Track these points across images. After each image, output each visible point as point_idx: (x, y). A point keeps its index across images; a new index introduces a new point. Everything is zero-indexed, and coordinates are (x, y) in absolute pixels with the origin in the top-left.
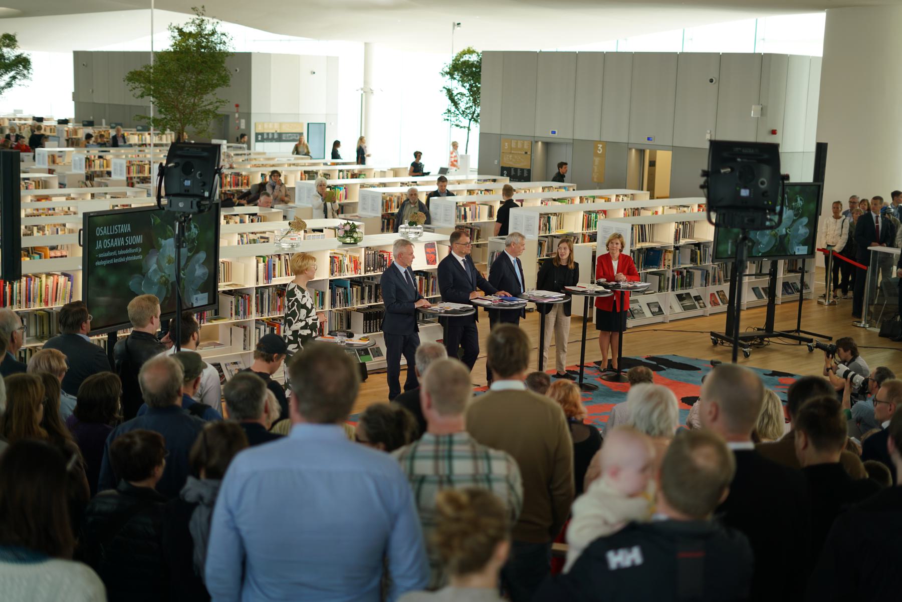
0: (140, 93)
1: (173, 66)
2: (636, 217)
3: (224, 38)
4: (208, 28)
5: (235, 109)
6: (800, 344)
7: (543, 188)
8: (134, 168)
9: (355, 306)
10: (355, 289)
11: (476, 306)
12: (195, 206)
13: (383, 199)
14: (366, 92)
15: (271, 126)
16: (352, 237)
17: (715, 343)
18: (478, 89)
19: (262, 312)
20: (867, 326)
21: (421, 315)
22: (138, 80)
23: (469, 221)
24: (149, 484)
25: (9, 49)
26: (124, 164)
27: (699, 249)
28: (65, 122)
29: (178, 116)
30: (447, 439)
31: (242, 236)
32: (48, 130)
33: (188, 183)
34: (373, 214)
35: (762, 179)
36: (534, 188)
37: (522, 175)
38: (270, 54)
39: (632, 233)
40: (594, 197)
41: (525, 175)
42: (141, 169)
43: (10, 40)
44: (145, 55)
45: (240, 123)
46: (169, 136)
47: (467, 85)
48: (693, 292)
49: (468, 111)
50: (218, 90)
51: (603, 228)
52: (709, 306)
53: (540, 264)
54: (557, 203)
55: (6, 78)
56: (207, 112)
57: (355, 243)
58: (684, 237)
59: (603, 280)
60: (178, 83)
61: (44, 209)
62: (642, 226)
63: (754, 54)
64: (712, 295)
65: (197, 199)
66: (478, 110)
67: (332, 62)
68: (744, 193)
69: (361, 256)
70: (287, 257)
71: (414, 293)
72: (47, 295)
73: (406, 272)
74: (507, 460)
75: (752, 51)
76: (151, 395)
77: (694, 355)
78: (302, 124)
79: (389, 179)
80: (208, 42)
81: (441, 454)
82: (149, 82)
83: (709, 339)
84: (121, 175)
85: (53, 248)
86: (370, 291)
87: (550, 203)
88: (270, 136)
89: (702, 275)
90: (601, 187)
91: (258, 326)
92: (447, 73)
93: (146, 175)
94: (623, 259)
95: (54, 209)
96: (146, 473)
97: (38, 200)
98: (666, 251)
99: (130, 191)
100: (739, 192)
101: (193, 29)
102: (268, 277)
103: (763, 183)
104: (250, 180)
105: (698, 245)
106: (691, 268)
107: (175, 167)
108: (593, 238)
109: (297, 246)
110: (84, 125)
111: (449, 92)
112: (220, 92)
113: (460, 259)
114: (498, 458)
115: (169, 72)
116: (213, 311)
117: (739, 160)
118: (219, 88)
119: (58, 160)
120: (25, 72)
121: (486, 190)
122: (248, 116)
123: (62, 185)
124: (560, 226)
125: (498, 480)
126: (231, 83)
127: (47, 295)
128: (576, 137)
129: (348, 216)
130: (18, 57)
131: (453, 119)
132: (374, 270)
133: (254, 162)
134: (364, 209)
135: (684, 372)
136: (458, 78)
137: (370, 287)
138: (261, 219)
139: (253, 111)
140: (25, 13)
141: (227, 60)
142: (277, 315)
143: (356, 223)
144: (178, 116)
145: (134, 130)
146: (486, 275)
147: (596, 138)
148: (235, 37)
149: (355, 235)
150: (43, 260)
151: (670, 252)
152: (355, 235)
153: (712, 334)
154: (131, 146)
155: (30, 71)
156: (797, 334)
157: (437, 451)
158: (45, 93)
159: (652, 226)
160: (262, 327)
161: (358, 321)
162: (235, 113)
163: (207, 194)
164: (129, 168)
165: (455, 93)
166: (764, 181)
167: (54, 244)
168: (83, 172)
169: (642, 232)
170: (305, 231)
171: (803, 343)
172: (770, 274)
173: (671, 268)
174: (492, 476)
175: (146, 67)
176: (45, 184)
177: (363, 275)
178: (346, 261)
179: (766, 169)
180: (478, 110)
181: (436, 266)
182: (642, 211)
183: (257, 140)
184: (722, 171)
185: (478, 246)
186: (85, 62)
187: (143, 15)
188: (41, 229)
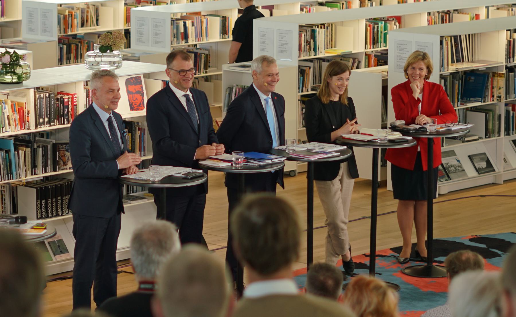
2: (447, 25)
9: (24, 179)
13: (59, 13)
16: (14, 73)
23: (192, 41)
34: (45, 38)
39: (441, 49)
54: (325, 9)
62: (455, 37)
69: (29, 101)
86: (45, 154)
87: (314, 9)
98: (494, 74)
108: (382, 59)
124: (331, 43)
132: (49, 122)
134: (31, 30)
143: (20, 52)
149: (19, 71)
151: (500, 75)
152: (19, 71)
159: (471, 37)
161: (29, 201)
169: (457, 47)
173: (504, 101)
177: (33, 130)
182: (455, 16)
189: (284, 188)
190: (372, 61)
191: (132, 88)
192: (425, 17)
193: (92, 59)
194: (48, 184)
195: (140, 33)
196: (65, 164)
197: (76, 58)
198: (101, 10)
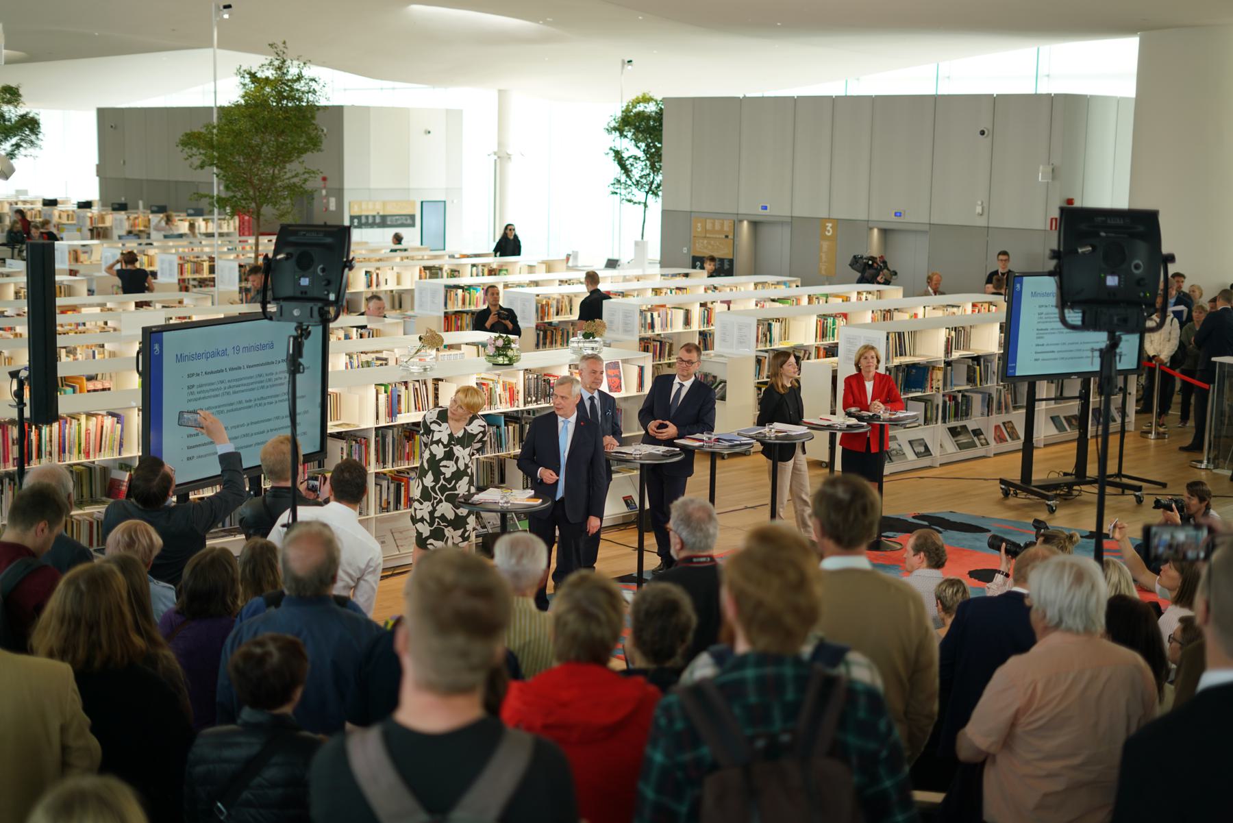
1: (244, 124)
2: (888, 322)
3: (313, 84)
4: (293, 71)
5: (322, 183)
6: (1123, 493)
7: (756, 285)
8: (188, 266)
9: (512, 452)
10: (511, 428)
12: (316, 313)
13: (537, 303)
14: (502, 158)
15: (371, 206)
17: (1006, 494)
18: (658, 150)
19: (384, 462)
20: (1211, 466)
22: (196, 145)
23: (658, 330)
24: (287, 709)
25: (11, 107)
26: (176, 261)
27: (979, 364)
28: (87, 205)
29: (251, 193)
32: (64, 216)
33: (305, 282)
35: (1137, 261)
36: (742, 284)
37: (724, 268)
38: (367, 109)
40: (827, 296)
41: (726, 266)
42: (197, 268)
43: (12, 94)
44: (208, 110)
45: (328, 202)
47: (643, 145)
48: (971, 424)
50: (307, 157)
51: (848, 339)
52: (993, 443)
53: (759, 389)
54: (777, 305)
55: (7, 146)
56: (292, 188)
57: (510, 364)
58: (957, 348)
59: (853, 410)
60: (252, 148)
61: (70, 325)
62: (899, 334)
64: (997, 427)
65: (320, 305)
66: (658, 179)
67: (453, 116)
68: (1112, 281)
69: (519, 382)
70: (417, 385)
72: (88, 443)
73: (592, 399)
76: (297, 580)
77: (979, 513)
79: (540, 275)
80: (292, 89)
82: (212, 147)
83: (996, 490)
84: (171, 275)
85: (90, 378)
87: (768, 305)
88: (370, 220)
89: (983, 400)
90: (830, 281)
91: (380, 481)
92: (615, 129)
93: (205, 274)
94: (879, 378)
95: (84, 324)
96: (285, 698)
98: (934, 368)
99: (188, 298)
101: (270, 73)
102: (393, 411)
103: (1137, 267)
105: (977, 359)
106: (967, 391)
107: (286, 259)
108: (832, 351)
109: (431, 369)
110: (114, 209)
111: (618, 156)
112: (311, 159)
114: (859, 664)
115: (238, 134)
117: (1103, 234)
119: (82, 257)
120: (33, 137)
122: (339, 193)
123: (91, 292)
124: (785, 335)
126: (323, 147)
127: (88, 443)
128: (796, 214)
130: (23, 117)
131: (623, 192)
132: (536, 401)
135: (968, 535)
136: (630, 135)
138: (373, 334)
139: (347, 185)
140: (32, 57)
141: (318, 115)
142: (404, 466)
144: (251, 193)
145: (183, 216)
147: (823, 214)
148: (330, 86)
150: (78, 394)
151: (939, 369)
152: (510, 353)
153: (1002, 481)
154: (181, 236)
155: (40, 136)
156: (1118, 480)
158: (60, 167)
159: (913, 334)
160: (385, 483)
163: (332, 297)
164: (181, 267)
165: (625, 155)
166: (1139, 264)
167: (93, 373)
169: (900, 342)
171: (1127, 492)
172: (1079, 397)
177: (522, 407)
178: (499, 390)
179: (1142, 247)
180: (658, 179)
182: (896, 314)
187: (203, 56)
188: (71, 351)
190: (822, 353)
191: (611, 372)
192: (869, 314)
193: (575, 345)
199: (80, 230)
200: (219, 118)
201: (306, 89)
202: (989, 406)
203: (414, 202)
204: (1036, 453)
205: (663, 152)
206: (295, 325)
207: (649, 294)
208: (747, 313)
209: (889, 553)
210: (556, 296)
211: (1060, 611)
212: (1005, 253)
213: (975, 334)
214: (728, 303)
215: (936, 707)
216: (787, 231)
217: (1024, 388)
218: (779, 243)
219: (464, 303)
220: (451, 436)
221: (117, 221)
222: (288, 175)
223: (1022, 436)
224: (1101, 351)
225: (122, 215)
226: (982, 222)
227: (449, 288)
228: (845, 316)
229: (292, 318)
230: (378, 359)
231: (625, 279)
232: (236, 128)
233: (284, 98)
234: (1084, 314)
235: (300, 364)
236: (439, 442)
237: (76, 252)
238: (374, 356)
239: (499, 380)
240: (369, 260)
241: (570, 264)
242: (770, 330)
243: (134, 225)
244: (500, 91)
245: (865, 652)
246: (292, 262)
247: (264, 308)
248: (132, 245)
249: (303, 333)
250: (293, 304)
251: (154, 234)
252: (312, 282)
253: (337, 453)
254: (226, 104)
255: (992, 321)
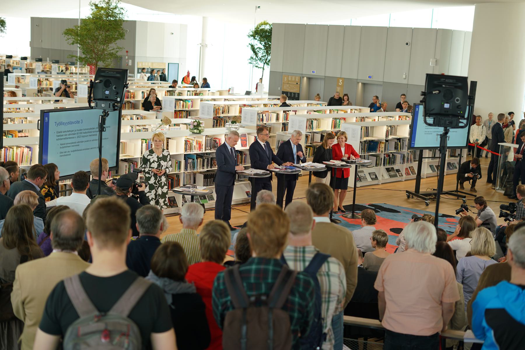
0: (72, 42)
1: (92, 26)
2: (363, 122)
3: (122, 10)
4: (113, 5)
6: (458, 199)
7: (308, 104)
9: (199, 170)
10: (199, 160)
11: (271, 172)
12: (111, 106)
13: (214, 108)
14: (203, 46)
15: (147, 64)
16: (198, 129)
21: (237, 175)
22: (70, 34)
23: (265, 122)
27: (400, 142)
28: (25, 58)
29: (94, 56)
30: (302, 250)
31: (132, 127)
32: (15, 63)
33: (107, 92)
34: (208, 117)
35: (457, 98)
37: (295, 97)
39: (361, 131)
40: (338, 110)
41: (296, 96)
46: (86, 69)
47: (263, 43)
48: (396, 167)
49: (263, 58)
50: (118, 41)
52: (404, 175)
54: (316, 113)
56: (111, 54)
60: (95, 37)
61: (14, 109)
63: (431, 29)
66: (269, 58)
68: (447, 106)
69: (203, 140)
71: (234, 162)
73: (231, 149)
74: (339, 265)
75: (429, 27)
77: (397, 204)
78: (164, 64)
79: (217, 96)
80: (113, 12)
81: (298, 258)
82: (77, 35)
83: (405, 194)
85: (20, 132)
86: (208, 162)
87: (312, 113)
89: (401, 157)
92: (252, 36)
95: (20, 109)
97: (10, 103)
98: (381, 142)
100: (443, 105)
101: (104, 5)
103: (457, 100)
104: (136, 95)
105: (399, 139)
107: (100, 82)
110: (36, 61)
113: (262, 144)
114: (333, 263)
115: (89, 30)
116: (115, 171)
117: (444, 86)
118: (119, 40)
119: (21, 81)
120: (2, 28)
121: (274, 104)
122: (133, 58)
123: (24, 95)
124: (318, 126)
125: (333, 276)
129: (193, 117)
131: (254, 63)
132: (210, 149)
133: (137, 85)
134: (203, 114)
136: (258, 38)
137: (208, 159)
138: (143, 118)
139: (136, 55)
141: (123, 24)
143: (201, 122)
144: (94, 56)
146: (275, 152)
148: (129, 12)
149: (200, 128)
150: (14, 138)
151: (383, 143)
152: (200, 128)
153: (407, 192)
157: (296, 256)
158: (15, 43)
159: (372, 128)
161: (200, 178)
162: (125, 56)
163: (119, 99)
165: (256, 47)
166: (458, 100)
167: (21, 129)
168: (36, 88)
169: (367, 131)
170: (170, 126)
171: (459, 198)
173: (383, 153)
174: (330, 273)
175: (75, 26)
176: (13, 94)
177: (204, 152)
178: (194, 144)
179: (460, 92)
180: (269, 58)
181: (248, 147)
182: (366, 119)
183: (138, 72)
184: (434, 92)
185: (270, 137)
186: (37, 24)
188: (12, 120)
189: (400, 212)
191: (243, 138)
193: (228, 126)
194: (208, 173)
195: (245, 117)
196: (215, 166)
197: (220, 125)
198: (230, 108)
199: (21, 69)
200: (81, 23)
201: (119, 12)
202: (403, 160)
203: (165, 63)
204: (422, 180)
205: (272, 47)
206: (102, 110)
207: (262, 106)
208: (303, 116)
209: (357, 220)
210: (223, 106)
211: (413, 242)
212: (404, 95)
213: (399, 129)
214: (295, 111)
215: (356, 281)
216: (323, 82)
217: (418, 153)
218: (319, 87)
219: (183, 107)
220: (158, 157)
221: (38, 66)
222: (110, 49)
223: (416, 173)
224: (441, 135)
225: (40, 63)
226: (405, 82)
227: (177, 100)
228: (345, 119)
229: (101, 108)
230: (144, 129)
231: (253, 100)
232: (88, 28)
233: (109, 16)
234: (434, 119)
235: (104, 127)
236: (154, 162)
237: (18, 78)
238: (142, 127)
239: (195, 140)
240: (144, 87)
241: (230, 92)
242: (312, 123)
243: (45, 68)
244: (203, 17)
245: (337, 258)
246: (102, 84)
247: (90, 105)
248: (43, 76)
249: (105, 115)
250: (102, 102)
251: (53, 72)
252: (110, 93)
253: (124, 169)
254: (84, 18)
255: (406, 124)
